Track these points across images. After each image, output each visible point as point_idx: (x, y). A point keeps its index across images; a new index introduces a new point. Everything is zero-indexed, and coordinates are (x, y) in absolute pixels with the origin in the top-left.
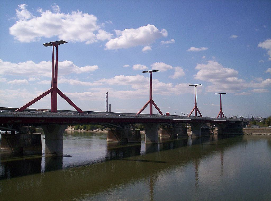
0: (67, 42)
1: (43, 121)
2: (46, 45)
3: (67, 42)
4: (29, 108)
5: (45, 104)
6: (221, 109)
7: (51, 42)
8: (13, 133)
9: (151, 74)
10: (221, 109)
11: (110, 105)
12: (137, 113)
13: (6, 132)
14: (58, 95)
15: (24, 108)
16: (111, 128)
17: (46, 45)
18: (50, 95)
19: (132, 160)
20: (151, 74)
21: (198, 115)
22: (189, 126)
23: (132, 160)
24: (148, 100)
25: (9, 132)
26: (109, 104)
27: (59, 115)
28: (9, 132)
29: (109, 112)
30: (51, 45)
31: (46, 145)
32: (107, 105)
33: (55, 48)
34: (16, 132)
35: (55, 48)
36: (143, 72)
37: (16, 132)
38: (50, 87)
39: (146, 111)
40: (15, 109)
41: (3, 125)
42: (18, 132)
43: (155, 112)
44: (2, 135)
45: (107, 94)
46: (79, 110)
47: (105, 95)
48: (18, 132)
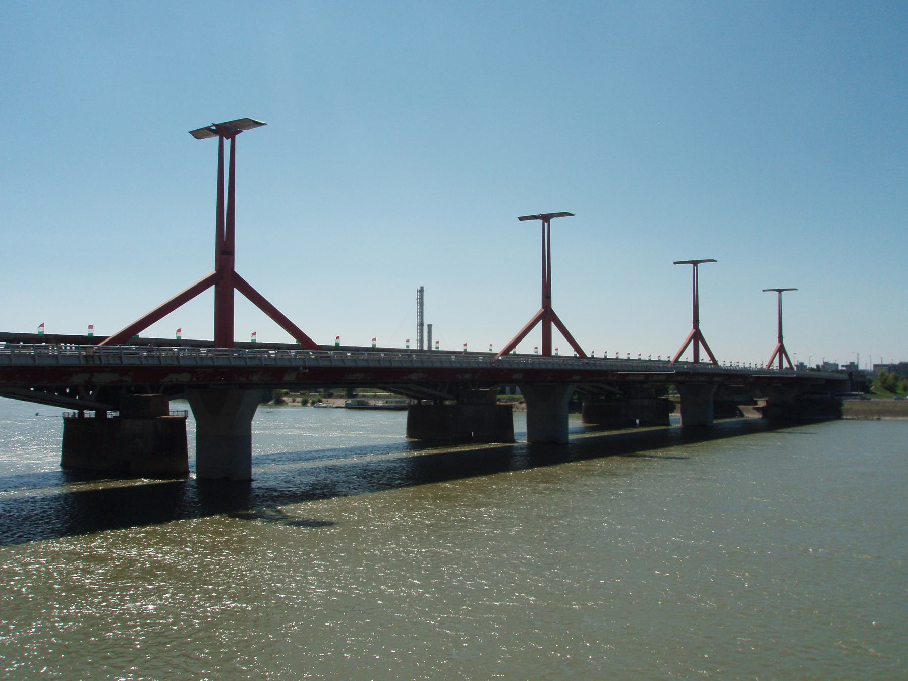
0: (262, 124)
1: (185, 378)
2: (199, 134)
3: (262, 124)
4: (143, 334)
5: (196, 323)
6: (781, 337)
7: (214, 125)
8: (101, 414)
9: (546, 225)
10: (781, 337)
11: (430, 326)
12: (498, 349)
13: (419, 402)
14: (238, 296)
15: (129, 335)
16: (419, 399)
17: (199, 134)
18: (211, 291)
19: (660, 457)
20: (546, 225)
21: (704, 357)
22: (674, 396)
23: (660, 457)
24: (537, 307)
25: (89, 414)
26: (426, 323)
27: (234, 359)
28: (89, 414)
29: (434, 349)
30: (215, 132)
31: (38, 471)
32: (422, 325)
33: (227, 143)
34: (111, 414)
35: (227, 143)
36: (521, 219)
37: (111, 414)
38: (210, 270)
39: (531, 346)
40: (101, 339)
41: (68, 391)
42: (117, 414)
43: (561, 348)
44: (67, 421)
45: (421, 291)
46: (304, 341)
47: (415, 296)
48: (117, 414)
